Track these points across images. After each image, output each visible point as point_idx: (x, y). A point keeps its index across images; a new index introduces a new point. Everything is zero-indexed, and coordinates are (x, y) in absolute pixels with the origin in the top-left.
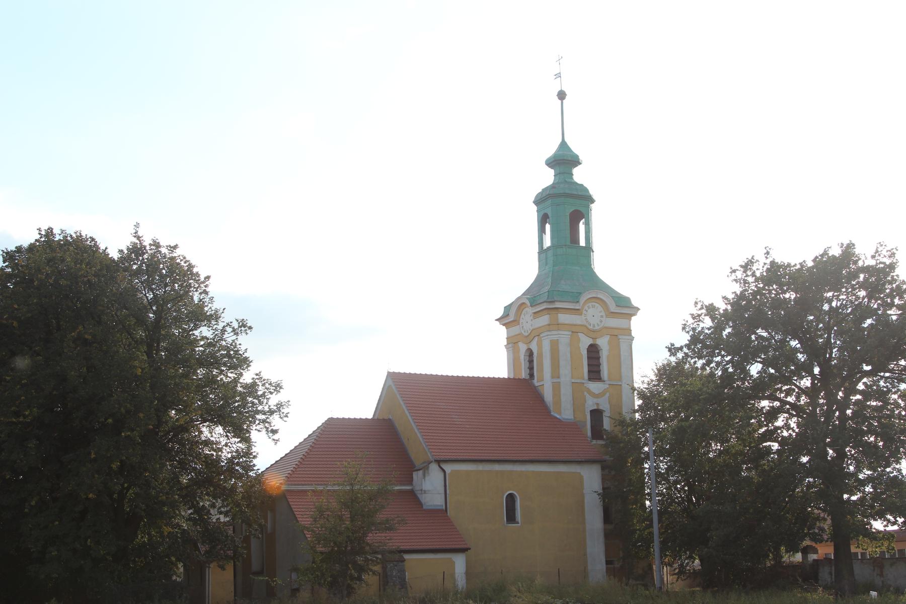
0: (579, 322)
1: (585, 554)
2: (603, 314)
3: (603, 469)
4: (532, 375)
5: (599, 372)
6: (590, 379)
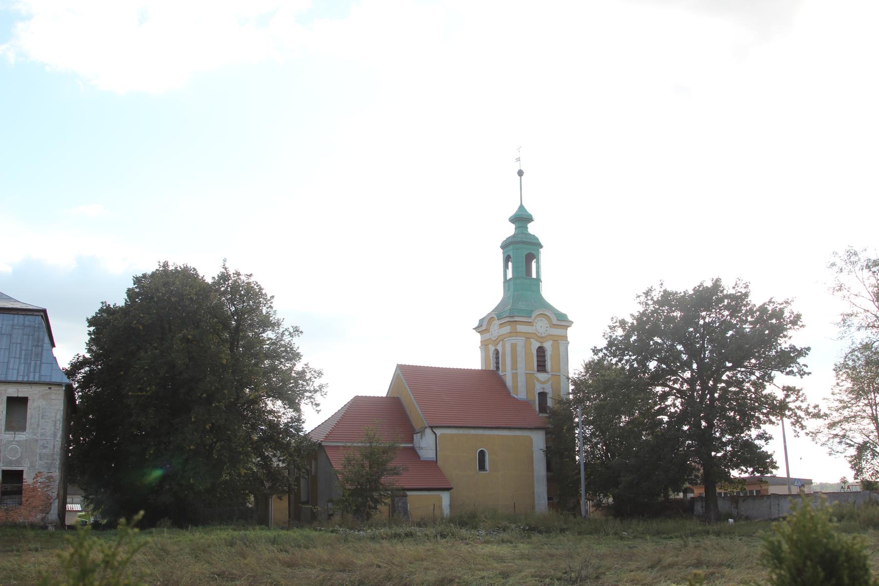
1: (533, 493)
4: (498, 368)
5: (544, 366)
6: (538, 371)
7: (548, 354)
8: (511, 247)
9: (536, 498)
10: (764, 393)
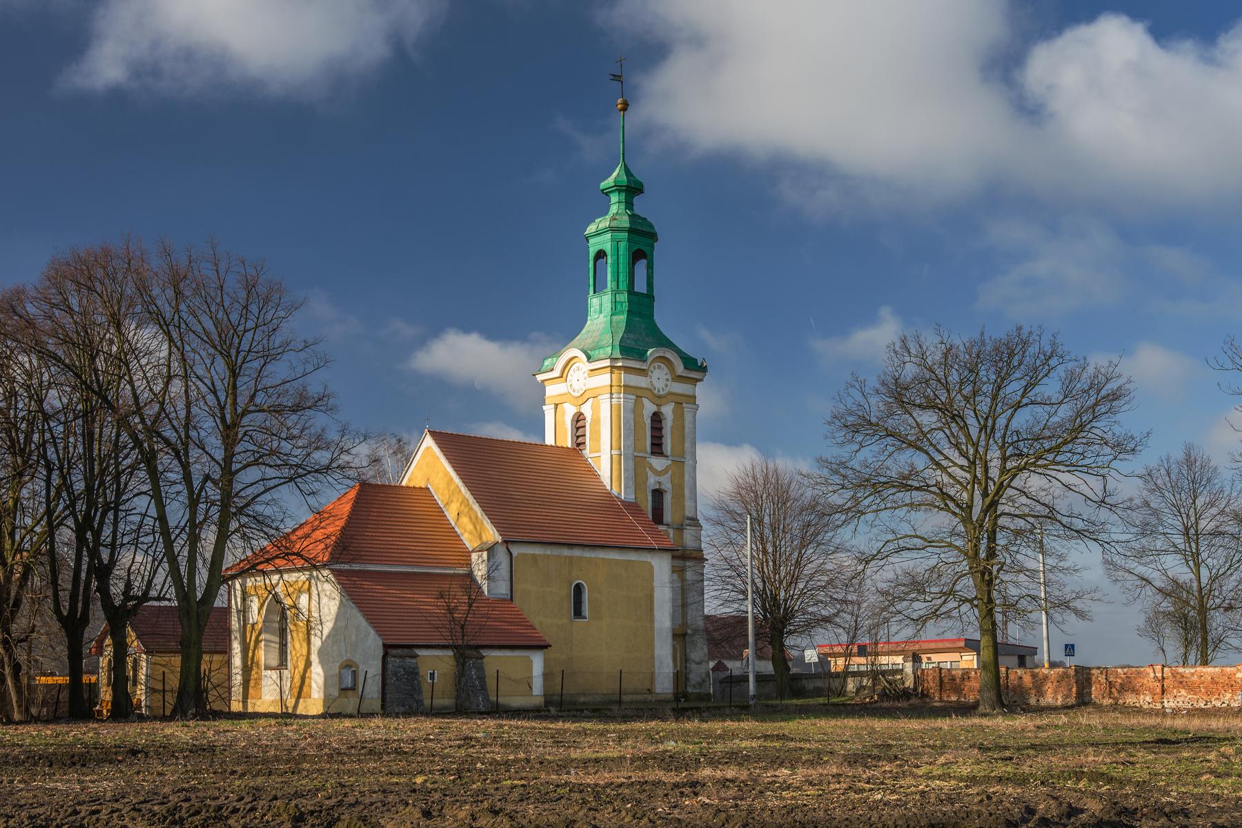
0: (643, 385)
1: (653, 657)
2: (669, 377)
3: (674, 557)
4: (579, 444)
5: (660, 445)
6: (653, 453)
7: (668, 424)
8: (609, 236)
9: (657, 664)
10: (604, 460)
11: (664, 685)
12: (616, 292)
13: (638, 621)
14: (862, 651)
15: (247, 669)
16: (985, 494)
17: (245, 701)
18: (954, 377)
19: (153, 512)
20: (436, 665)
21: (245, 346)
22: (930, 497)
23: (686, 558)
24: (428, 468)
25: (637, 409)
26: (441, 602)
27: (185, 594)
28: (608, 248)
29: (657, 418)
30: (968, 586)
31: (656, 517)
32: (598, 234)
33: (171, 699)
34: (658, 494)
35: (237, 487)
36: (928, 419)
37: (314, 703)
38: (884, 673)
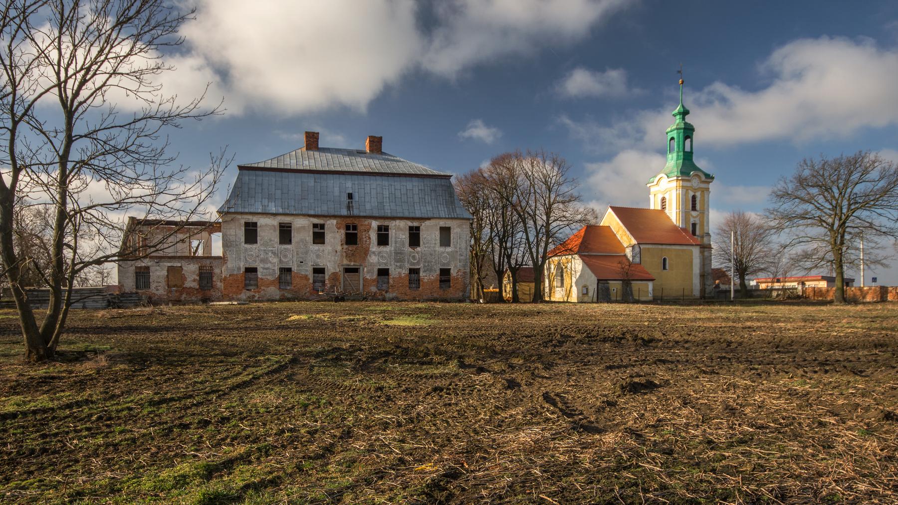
4: (663, 208)
10: (674, 214)
11: (697, 293)
12: (678, 152)
13: (686, 273)
14: (778, 281)
15: (550, 290)
16: (840, 219)
17: (550, 297)
18: (826, 174)
19: (524, 237)
20: (615, 286)
21: (553, 181)
22: (814, 221)
23: (705, 248)
24: (610, 220)
25: (685, 195)
26: (619, 265)
27: (535, 263)
28: (675, 136)
29: (694, 198)
30: (830, 256)
31: (693, 233)
32: (671, 131)
33: (532, 297)
34: (694, 225)
35: (551, 227)
36: (814, 191)
37: (574, 298)
38: (789, 289)
